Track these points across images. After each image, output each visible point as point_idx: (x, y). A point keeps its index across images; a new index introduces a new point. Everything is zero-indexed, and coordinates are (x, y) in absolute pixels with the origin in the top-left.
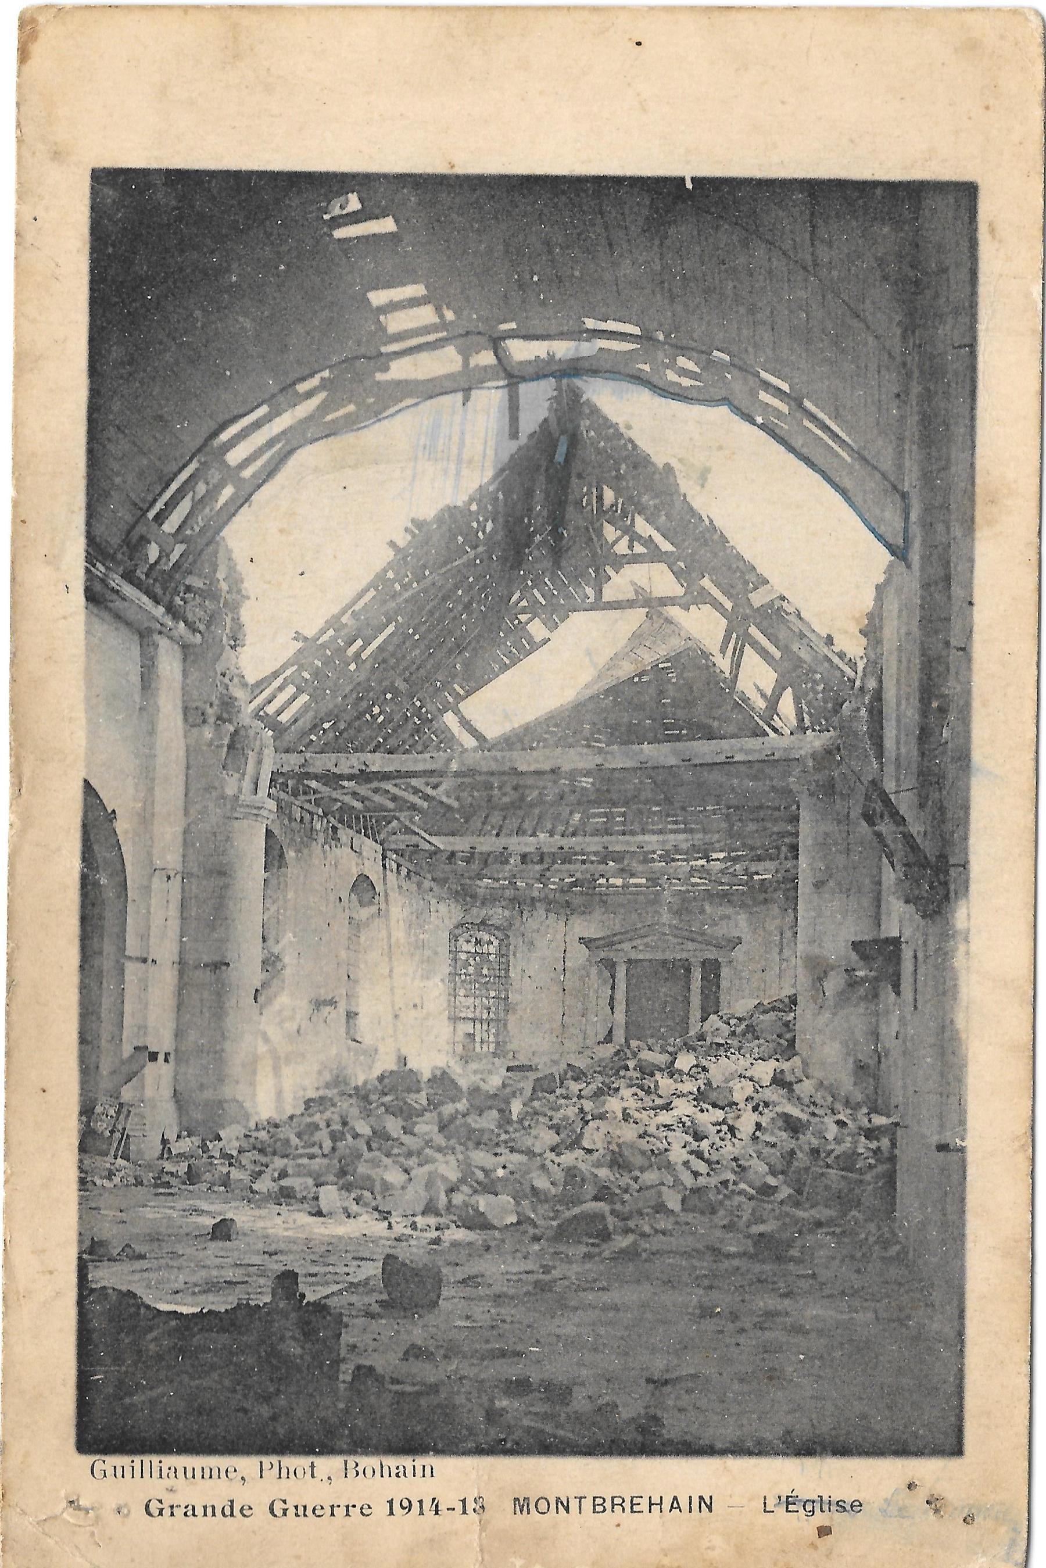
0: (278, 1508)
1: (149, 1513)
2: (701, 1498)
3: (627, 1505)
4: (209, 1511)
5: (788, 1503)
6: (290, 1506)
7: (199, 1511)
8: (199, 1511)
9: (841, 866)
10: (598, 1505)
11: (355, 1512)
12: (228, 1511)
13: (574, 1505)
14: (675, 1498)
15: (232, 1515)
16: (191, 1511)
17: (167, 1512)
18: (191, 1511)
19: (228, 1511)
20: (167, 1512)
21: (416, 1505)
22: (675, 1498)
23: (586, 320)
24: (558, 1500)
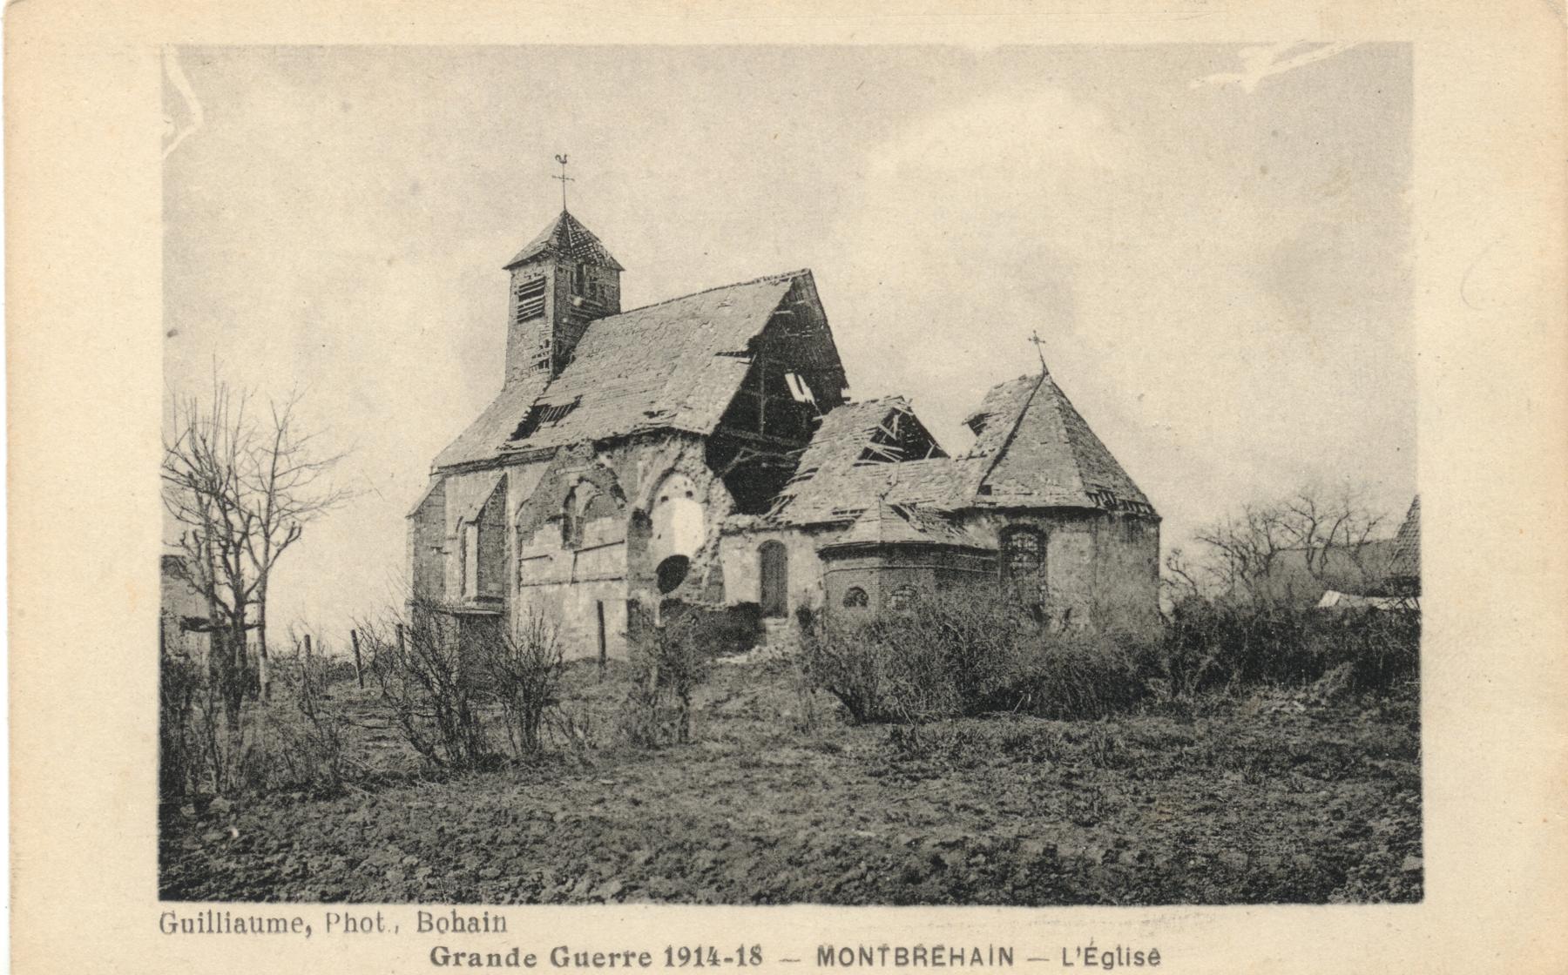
0: (560, 956)
1: (434, 960)
2: (1002, 950)
3: (929, 957)
4: (581, 960)
5: (1087, 957)
6: (571, 955)
7: (484, 960)
8: (484, 960)
9: (379, 885)
10: (901, 957)
11: (634, 961)
12: (512, 960)
13: (877, 956)
14: (976, 950)
15: (516, 964)
16: (475, 961)
17: (452, 960)
18: (475, 961)
19: (512, 960)
20: (452, 960)
21: (694, 957)
22: (976, 950)
23: (993, 543)
24: (862, 950)
